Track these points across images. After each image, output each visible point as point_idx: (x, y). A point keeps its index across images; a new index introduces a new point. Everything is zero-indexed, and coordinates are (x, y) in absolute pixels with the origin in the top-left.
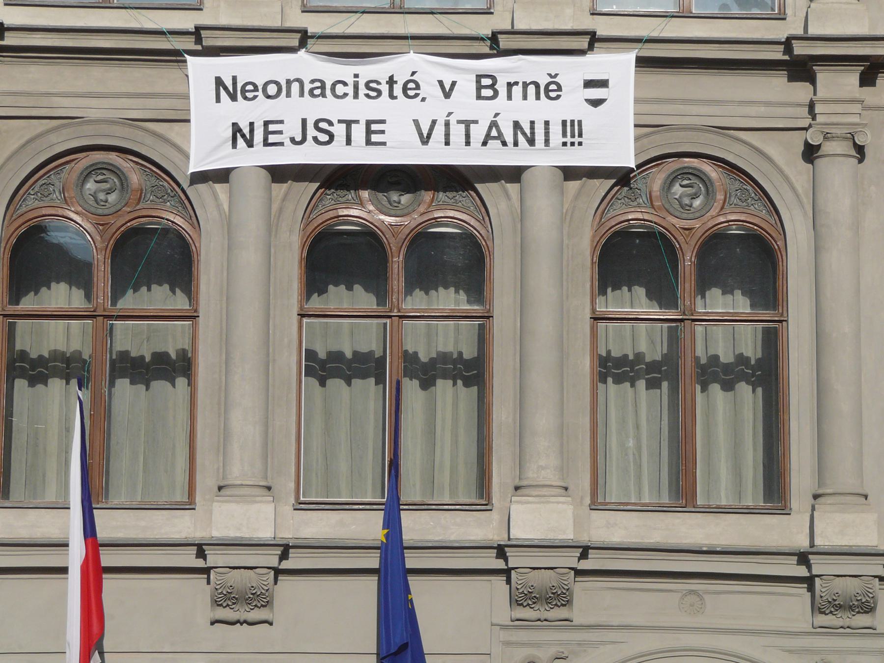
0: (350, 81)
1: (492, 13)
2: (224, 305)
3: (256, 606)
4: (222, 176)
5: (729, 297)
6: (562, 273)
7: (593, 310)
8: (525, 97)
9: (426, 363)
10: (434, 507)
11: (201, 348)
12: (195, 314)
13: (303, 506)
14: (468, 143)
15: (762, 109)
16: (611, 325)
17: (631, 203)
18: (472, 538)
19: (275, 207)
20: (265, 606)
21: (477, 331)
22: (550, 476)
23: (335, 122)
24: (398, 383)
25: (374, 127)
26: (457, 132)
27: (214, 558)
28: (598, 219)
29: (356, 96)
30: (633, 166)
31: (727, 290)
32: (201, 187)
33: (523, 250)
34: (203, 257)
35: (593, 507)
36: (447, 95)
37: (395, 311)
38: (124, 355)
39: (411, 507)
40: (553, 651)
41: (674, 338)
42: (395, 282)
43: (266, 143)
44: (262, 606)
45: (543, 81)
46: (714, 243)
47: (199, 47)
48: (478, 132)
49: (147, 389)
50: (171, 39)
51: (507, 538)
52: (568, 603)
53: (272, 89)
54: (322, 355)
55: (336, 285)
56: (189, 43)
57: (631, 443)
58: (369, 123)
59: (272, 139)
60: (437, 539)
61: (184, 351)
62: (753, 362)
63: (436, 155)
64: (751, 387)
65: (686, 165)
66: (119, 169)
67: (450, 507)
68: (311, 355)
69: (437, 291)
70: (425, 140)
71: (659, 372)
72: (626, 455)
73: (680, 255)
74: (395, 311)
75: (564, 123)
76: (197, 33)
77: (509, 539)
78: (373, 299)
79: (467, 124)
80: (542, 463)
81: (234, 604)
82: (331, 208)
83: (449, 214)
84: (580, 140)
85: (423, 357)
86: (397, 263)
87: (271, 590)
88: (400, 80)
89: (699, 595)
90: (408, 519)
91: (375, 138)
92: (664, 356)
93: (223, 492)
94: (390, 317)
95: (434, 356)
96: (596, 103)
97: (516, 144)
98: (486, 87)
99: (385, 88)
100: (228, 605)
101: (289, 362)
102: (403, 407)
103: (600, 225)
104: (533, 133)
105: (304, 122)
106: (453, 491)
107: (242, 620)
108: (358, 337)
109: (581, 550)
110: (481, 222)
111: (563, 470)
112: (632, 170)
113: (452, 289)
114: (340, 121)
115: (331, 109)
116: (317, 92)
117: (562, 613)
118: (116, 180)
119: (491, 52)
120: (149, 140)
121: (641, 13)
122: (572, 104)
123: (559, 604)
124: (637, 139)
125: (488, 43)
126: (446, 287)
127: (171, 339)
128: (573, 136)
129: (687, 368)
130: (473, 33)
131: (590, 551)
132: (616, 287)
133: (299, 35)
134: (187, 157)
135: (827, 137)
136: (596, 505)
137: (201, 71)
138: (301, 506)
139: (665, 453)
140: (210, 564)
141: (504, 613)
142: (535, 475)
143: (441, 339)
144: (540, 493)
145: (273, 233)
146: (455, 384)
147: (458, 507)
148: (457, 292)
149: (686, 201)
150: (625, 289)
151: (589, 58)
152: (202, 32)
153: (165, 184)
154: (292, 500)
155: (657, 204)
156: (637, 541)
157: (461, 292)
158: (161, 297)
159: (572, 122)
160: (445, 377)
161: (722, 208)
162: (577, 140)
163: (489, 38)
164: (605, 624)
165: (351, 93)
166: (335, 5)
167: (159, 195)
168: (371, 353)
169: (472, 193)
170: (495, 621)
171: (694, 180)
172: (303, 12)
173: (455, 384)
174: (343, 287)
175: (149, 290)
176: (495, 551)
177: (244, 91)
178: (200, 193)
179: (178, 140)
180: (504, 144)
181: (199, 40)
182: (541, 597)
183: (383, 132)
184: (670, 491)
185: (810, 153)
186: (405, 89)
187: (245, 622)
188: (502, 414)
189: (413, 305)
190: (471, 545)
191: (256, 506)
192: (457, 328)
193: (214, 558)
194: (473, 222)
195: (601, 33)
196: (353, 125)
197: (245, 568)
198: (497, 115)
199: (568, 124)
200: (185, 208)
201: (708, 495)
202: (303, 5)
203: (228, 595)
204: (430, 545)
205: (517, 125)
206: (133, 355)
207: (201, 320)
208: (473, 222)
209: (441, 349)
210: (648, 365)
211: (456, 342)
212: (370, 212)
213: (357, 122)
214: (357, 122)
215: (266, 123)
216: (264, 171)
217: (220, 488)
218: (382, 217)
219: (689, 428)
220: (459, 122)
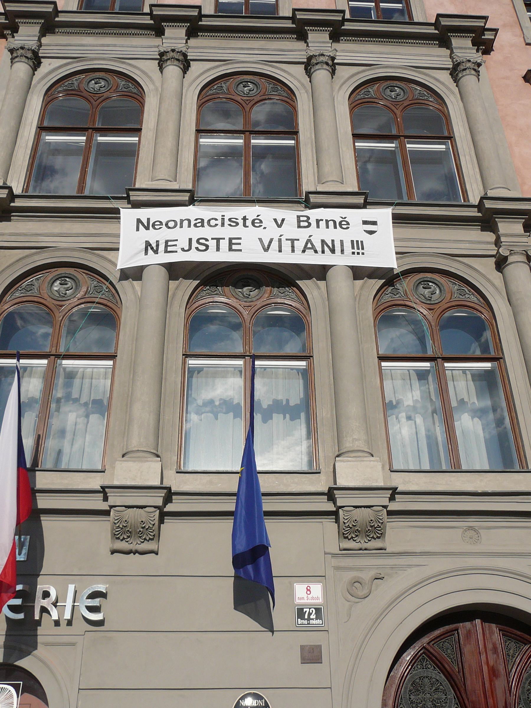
0: (220, 218)
8: (327, 227)
14: (293, 251)
15: (467, 245)
20: (152, 539)
23: (210, 239)
25: (234, 241)
26: (286, 246)
29: (223, 225)
34: (122, 320)
36: (279, 226)
40: (372, 573)
43: (166, 251)
44: (150, 539)
48: (299, 245)
52: (381, 536)
53: (171, 224)
58: (230, 240)
63: (272, 257)
75: (352, 242)
79: (293, 241)
83: (281, 302)
84: (363, 251)
91: (234, 247)
96: (371, 233)
97: (323, 252)
98: (303, 221)
99: (241, 222)
104: (333, 245)
105: (190, 240)
109: (391, 492)
114: (212, 239)
117: (377, 544)
122: (357, 232)
123: (375, 537)
135: (512, 252)
142: (351, 445)
146: (285, 418)
159: (357, 241)
162: (361, 251)
169: (295, 289)
170: (327, 551)
177: (154, 225)
179: (113, 260)
180: (316, 252)
182: (362, 529)
183: (240, 244)
185: (501, 263)
191: (147, 464)
193: (114, 499)
198: (310, 236)
199: (355, 242)
205: (323, 242)
216: (163, 269)
220: (287, 240)
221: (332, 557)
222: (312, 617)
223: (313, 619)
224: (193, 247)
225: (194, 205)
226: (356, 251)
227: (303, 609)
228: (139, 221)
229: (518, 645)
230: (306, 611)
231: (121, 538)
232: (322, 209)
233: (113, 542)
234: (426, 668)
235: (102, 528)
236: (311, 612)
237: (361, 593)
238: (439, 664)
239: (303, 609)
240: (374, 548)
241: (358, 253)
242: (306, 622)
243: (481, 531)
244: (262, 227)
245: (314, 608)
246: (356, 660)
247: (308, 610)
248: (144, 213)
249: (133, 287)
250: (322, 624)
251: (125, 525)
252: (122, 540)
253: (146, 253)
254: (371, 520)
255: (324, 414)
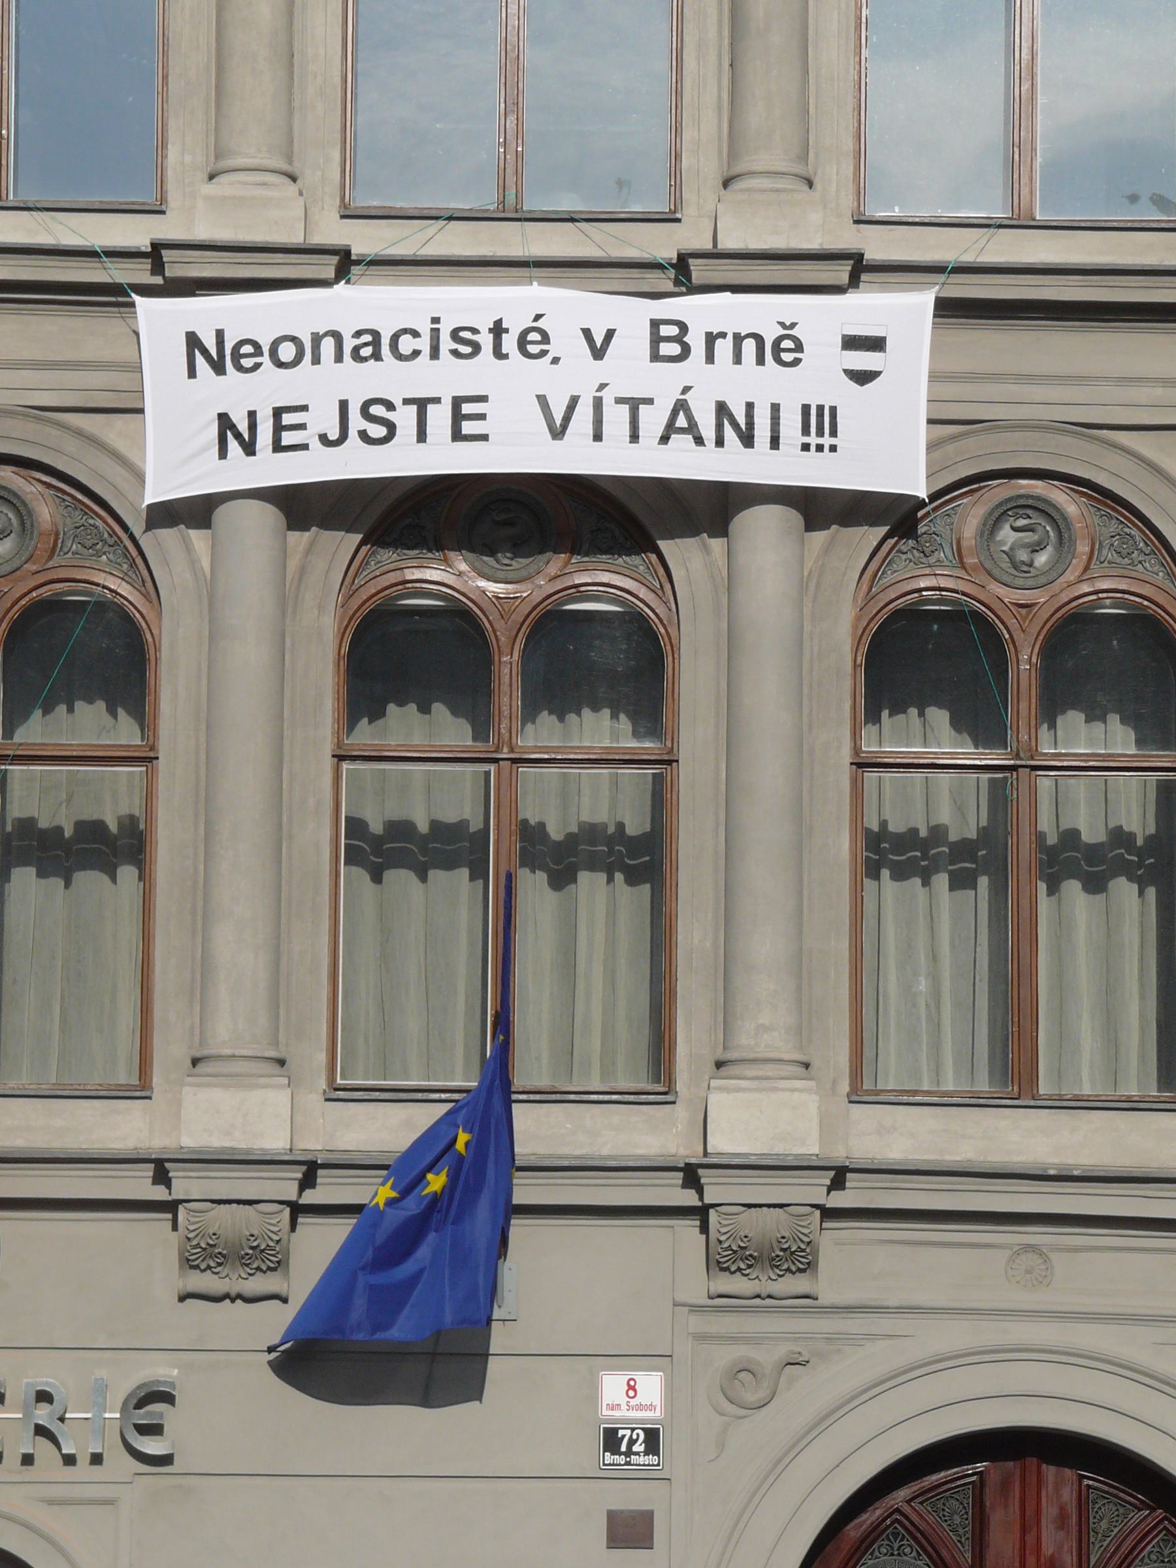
0: (425, 328)
1: (678, 220)
2: (203, 739)
3: (258, 1269)
4: (197, 512)
5: (1098, 727)
6: (801, 685)
7: (857, 750)
8: (738, 359)
9: (559, 843)
10: (572, 1097)
11: (162, 814)
12: (152, 754)
13: (341, 1094)
14: (634, 437)
16: (888, 775)
17: (924, 560)
18: (640, 1152)
19: (293, 564)
20: (274, 1269)
21: (650, 786)
22: (778, 1043)
23: (398, 402)
24: (509, 877)
27: (184, 1184)
28: (865, 588)
29: (435, 353)
30: (923, 494)
31: (1095, 714)
32: (168, 536)
33: (732, 643)
35: (855, 1098)
36: (598, 353)
37: (505, 750)
38: (27, 825)
39: (532, 1097)
40: (782, 1351)
41: (999, 799)
42: (506, 700)
43: (278, 447)
44: (270, 1269)
45: (770, 334)
46: (1072, 630)
47: (158, 280)
48: (653, 420)
49: (67, 886)
50: (109, 265)
51: (701, 1154)
52: (810, 1267)
53: (287, 352)
54: (376, 827)
55: (401, 703)
56: (140, 273)
57: (923, 985)
58: (457, 402)
59: (288, 438)
60: (578, 1152)
61: (133, 819)
62: (1140, 842)
64: (1136, 886)
65: (1022, 492)
66: (15, 495)
67: (601, 1097)
68: (356, 827)
69: (580, 715)
70: (558, 432)
71: (973, 860)
72: (914, 1005)
73: (1010, 649)
74: (505, 750)
75: (806, 409)
76: (156, 253)
77: (706, 1154)
78: (468, 729)
79: (634, 404)
80: (765, 1019)
81: (219, 1264)
82: (392, 566)
83: (603, 583)
84: (833, 441)
85: (555, 832)
86: (508, 666)
87: (284, 1242)
88: (515, 326)
89: (1042, 1254)
90: (524, 1118)
91: (468, 427)
92: (983, 832)
93: (201, 1068)
94: (496, 761)
95: (574, 829)
96: (862, 377)
97: (720, 442)
98: (668, 339)
99: (486, 340)
100: (209, 1267)
101: (317, 838)
102: (519, 919)
103: (870, 598)
104: (750, 424)
105: (344, 406)
106: (607, 1071)
107: (233, 1294)
108: (443, 794)
109: (832, 1173)
110: (658, 593)
111: (801, 1031)
112: (922, 504)
113: (606, 712)
114: (407, 402)
115: (387, 379)
116: (366, 352)
118: (11, 515)
119: (677, 290)
120: (71, 445)
121: (945, 220)
122: (820, 376)
123: (794, 1268)
124: (931, 447)
125: (672, 273)
126: (596, 709)
127: (110, 797)
128: (820, 433)
129: (1023, 852)
130: (646, 255)
131: (848, 1175)
132: (898, 709)
133: (335, 260)
134: (140, 477)
136: (859, 1095)
137: (161, 321)
138: (337, 1093)
139: (983, 1003)
140: (178, 1192)
141: (696, 1283)
142: (752, 1042)
143: (586, 800)
144: (760, 1073)
145: (290, 611)
146: (610, 880)
147: (614, 1097)
148: (614, 716)
149: (1023, 555)
150: (913, 712)
151: (851, 299)
152: (163, 252)
153: (99, 523)
154: (323, 1084)
155: (970, 560)
156: (932, 1157)
157: (622, 717)
158: (89, 724)
159: (820, 408)
160: (592, 868)
161: (1087, 568)
162: (827, 441)
163: (672, 265)
164: (873, 1303)
165: (426, 350)
166: (399, 205)
167: (89, 543)
168: (463, 824)
170: (680, 1298)
171: (1037, 519)
172: (343, 217)
173: (610, 880)
174: (412, 707)
175: (71, 710)
176: (681, 1174)
177: (237, 356)
178: (168, 549)
179: (120, 445)
180: (699, 441)
181: (158, 267)
182: (761, 1255)
183: (482, 417)
184: (991, 1073)
186: (522, 342)
187: (240, 1296)
188: (694, 934)
189: (536, 740)
190: (638, 1164)
191: (256, 1096)
192: (615, 782)
193: (184, 1184)
194: (643, 592)
195: (873, 254)
196: (430, 407)
197: (239, 1202)
198: (686, 390)
199: (813, 412)
200: (133, 564)
201: (1060, 1077)
202: (343, 205)
203: (209, 1250)
204: (566, 1163)
205: (722, 409)
206: (43, 824)
207: (162, 764)
208: (643, 592)
209: (586, 817)
210: (953, 846)
211: (613, 806)
212: (460, 574)
213: (437, 400)
214: (437, 400)
215: (278, 413)
217: (195, 1062)
218: (482, 583)
219: (1025, 960)
220: (619, 401)
221: (690, 1311)
222: (635, 1448)
223: (637, 1454)
224: (353, 433)
225: (348, 282)
226: (813, 440)
227: (616, 1430)
228: (193, 342)
229: (1121, 1510)
230: (624, 1436)
231: (203, 1266)
232: (729, 294)
233: (181, 1275)
234: (899, 1555)
235: (154, 1239)
236: (635, 1437)
237: (751, 1397)
238: (929, 1549)
239: (616, 1430)
240: (789, 1294)
241: (820, 448)
242: (621, 1459)
243: (1053, 1256)
244: (549, 357)
245: (642, 1429)
246: (726, 1547)
247: (628, 1432)
248: (207, 314)
249: (188, 547)
250: (658, 1465)
251: (211, 1242)
252: (203, 1271)
253: (223, 453)
254: (783, 1237)
255: (696, 941)
